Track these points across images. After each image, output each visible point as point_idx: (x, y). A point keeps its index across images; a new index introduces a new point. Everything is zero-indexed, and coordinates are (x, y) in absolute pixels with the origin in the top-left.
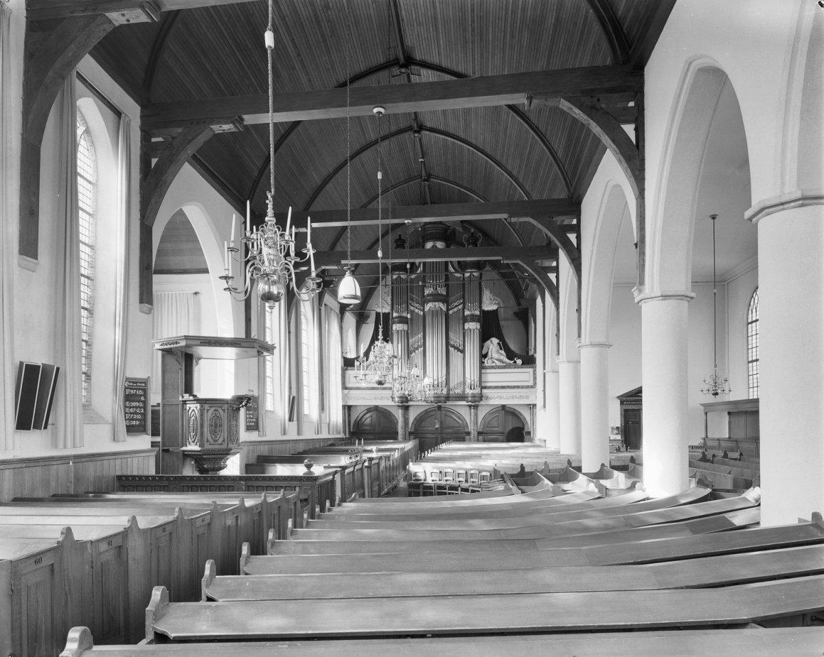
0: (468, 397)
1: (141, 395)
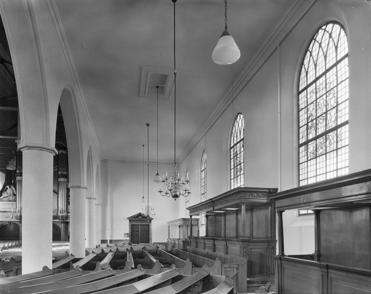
0: (59, 217)
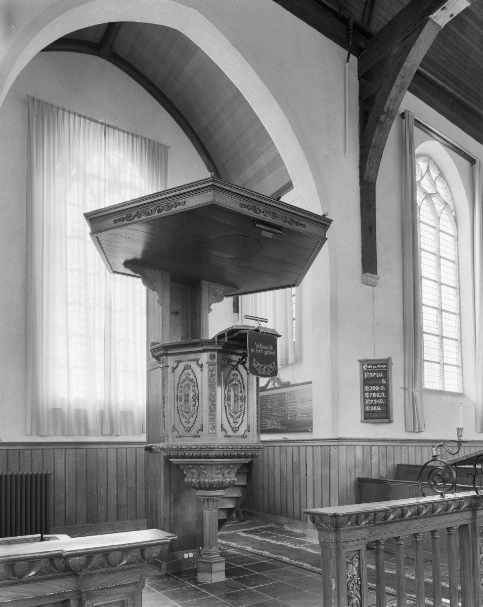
1: (381, 378)
